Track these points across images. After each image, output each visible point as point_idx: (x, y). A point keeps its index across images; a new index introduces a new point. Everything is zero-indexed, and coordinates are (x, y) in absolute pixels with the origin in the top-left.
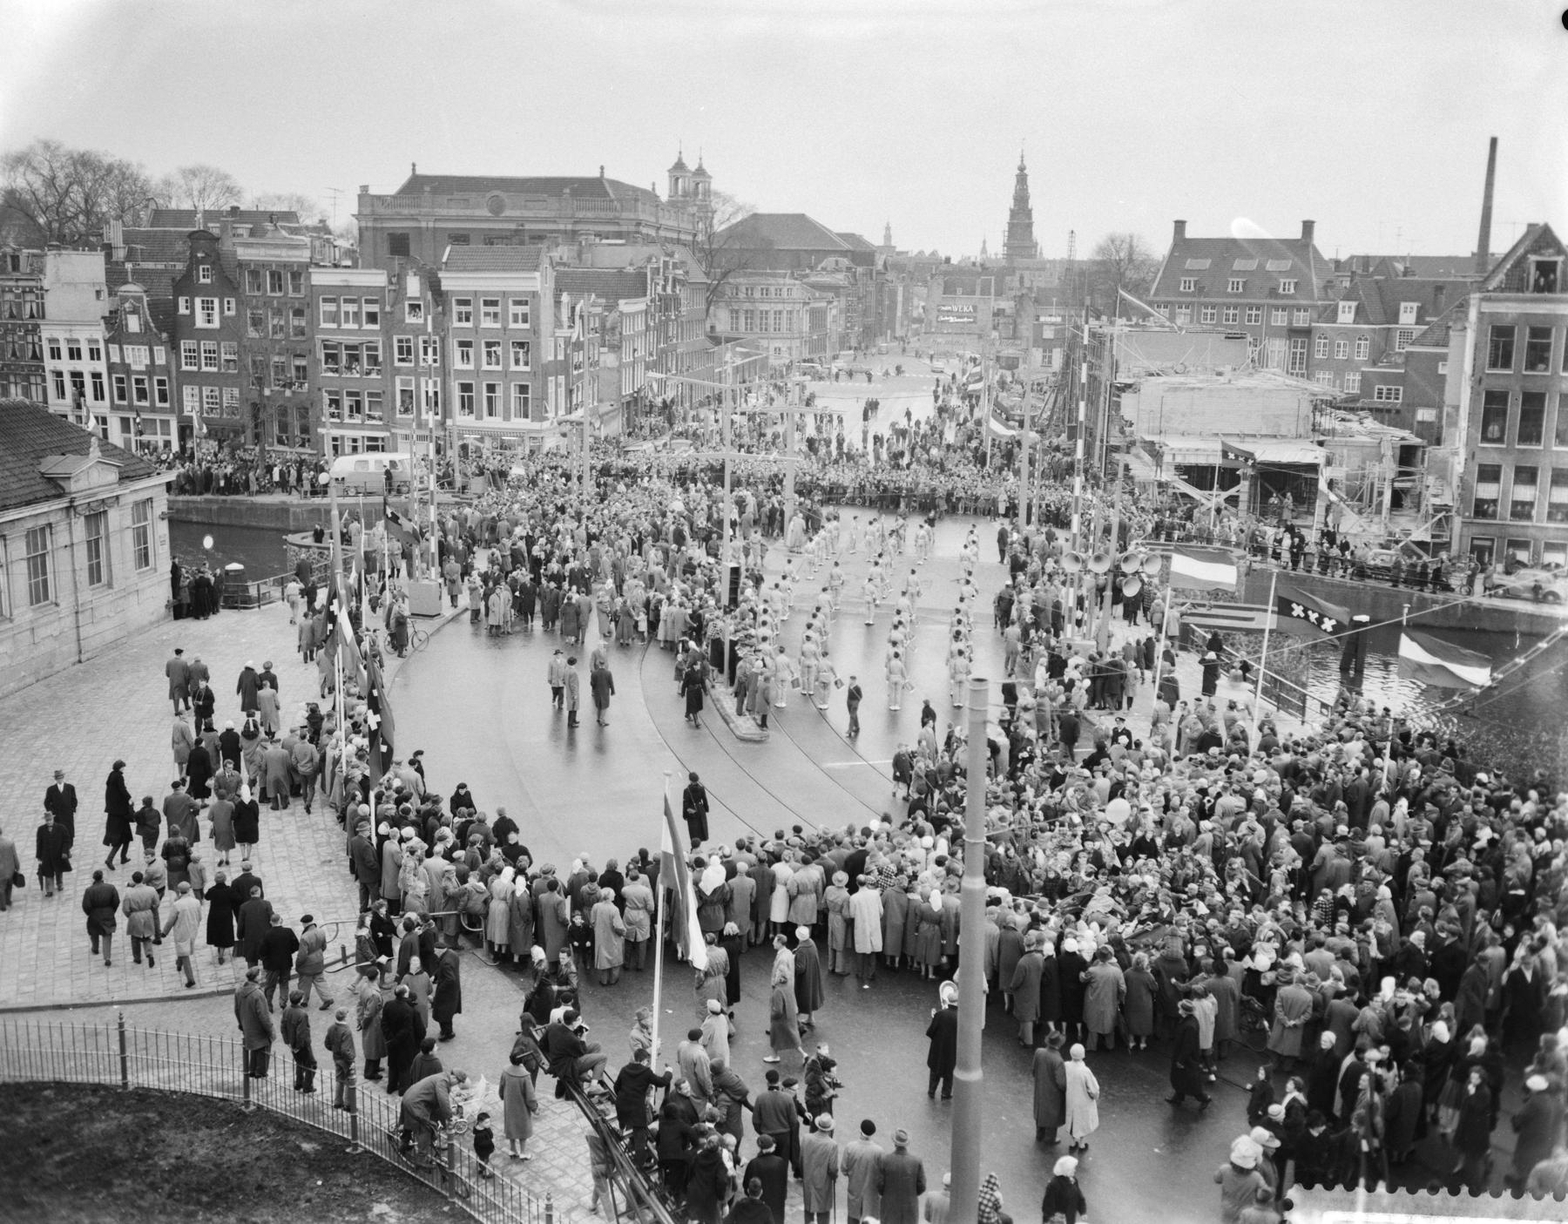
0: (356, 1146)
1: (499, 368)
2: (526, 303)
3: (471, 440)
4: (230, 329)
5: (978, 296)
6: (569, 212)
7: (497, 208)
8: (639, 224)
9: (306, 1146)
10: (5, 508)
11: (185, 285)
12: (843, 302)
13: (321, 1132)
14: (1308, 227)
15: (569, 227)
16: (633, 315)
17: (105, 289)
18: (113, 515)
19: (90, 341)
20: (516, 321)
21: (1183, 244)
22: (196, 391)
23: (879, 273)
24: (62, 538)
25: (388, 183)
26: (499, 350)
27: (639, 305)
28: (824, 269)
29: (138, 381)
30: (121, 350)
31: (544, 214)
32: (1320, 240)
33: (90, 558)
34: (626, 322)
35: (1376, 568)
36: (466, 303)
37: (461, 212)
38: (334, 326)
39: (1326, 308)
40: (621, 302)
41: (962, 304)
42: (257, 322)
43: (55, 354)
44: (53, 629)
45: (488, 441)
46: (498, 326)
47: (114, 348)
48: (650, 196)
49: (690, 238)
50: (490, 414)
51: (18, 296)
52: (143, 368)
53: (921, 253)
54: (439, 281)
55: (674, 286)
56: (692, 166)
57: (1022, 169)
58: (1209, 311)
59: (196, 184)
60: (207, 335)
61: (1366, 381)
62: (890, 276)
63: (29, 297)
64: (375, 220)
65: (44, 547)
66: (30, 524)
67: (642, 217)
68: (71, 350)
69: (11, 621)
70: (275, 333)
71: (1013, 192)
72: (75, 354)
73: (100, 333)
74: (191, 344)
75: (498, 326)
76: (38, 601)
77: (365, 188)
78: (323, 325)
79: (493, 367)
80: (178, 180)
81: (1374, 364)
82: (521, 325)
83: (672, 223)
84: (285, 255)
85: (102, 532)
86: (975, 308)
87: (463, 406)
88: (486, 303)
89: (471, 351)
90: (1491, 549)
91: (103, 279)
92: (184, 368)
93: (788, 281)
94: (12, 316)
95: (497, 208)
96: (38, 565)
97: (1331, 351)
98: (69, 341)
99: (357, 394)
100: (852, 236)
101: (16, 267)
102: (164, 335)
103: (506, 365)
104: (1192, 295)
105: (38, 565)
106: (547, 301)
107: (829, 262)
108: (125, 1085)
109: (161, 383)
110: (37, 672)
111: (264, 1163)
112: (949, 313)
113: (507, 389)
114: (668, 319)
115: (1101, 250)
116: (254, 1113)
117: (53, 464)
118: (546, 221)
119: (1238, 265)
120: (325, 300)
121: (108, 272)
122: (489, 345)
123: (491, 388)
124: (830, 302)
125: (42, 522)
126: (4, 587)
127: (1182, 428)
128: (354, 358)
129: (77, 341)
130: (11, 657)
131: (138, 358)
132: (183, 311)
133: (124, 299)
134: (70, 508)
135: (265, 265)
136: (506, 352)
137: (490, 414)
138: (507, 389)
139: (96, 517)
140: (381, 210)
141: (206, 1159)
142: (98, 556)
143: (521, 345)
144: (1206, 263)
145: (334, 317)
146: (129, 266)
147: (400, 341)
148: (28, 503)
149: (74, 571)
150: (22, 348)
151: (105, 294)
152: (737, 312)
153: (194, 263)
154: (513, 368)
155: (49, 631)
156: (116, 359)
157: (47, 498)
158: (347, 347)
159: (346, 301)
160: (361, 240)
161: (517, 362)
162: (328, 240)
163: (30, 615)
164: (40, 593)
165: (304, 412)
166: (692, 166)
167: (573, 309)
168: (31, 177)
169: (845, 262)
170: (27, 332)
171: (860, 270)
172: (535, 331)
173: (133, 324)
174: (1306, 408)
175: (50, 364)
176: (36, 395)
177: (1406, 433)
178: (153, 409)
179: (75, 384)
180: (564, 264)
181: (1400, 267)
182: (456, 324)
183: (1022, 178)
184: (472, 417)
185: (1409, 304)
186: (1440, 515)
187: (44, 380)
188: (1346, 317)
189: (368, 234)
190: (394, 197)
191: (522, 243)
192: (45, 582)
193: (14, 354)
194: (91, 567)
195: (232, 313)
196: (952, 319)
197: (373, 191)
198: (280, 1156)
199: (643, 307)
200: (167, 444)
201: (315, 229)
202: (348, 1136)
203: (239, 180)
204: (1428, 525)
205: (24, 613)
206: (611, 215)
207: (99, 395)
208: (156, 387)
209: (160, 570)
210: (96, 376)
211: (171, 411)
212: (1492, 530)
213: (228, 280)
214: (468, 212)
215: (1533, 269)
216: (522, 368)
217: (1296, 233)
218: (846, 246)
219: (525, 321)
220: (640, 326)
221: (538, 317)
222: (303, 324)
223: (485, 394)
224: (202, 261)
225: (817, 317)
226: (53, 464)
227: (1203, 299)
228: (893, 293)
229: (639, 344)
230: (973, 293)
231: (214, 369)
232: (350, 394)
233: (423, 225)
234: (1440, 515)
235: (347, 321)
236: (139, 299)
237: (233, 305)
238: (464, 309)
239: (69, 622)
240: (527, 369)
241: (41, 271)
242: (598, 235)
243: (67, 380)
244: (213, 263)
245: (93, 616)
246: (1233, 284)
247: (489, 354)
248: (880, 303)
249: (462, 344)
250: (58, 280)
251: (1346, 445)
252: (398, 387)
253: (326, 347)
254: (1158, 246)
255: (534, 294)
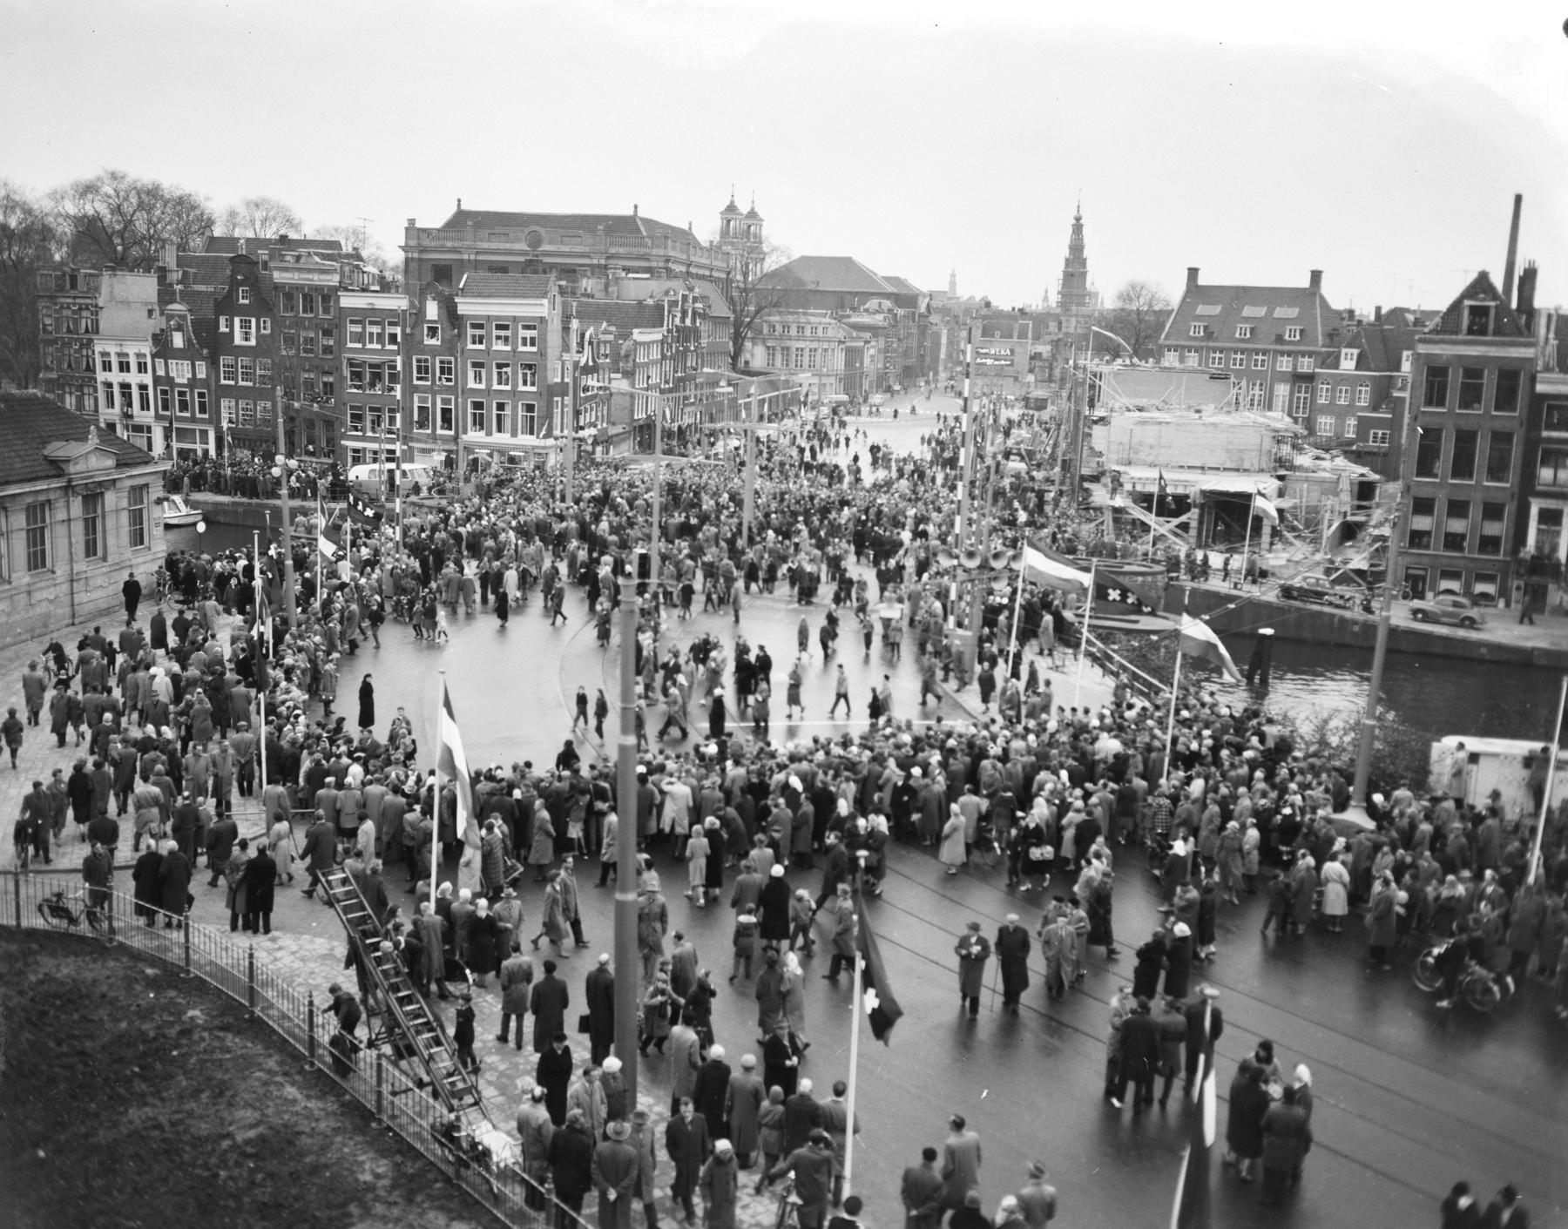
0: (188, 972)
1: (508, 388)
2: (534, 328)
3: (482, 454)
4: (265, 347)
5: (1015, 339)
6: (603, 248)
7: (535, 241)
8: (668, 261)
9: (149, 971)
10: (8, 483)
11: (226, 305)
12: (882, 343)
13: (164, 961)
14: (1316, 276)
15: (603, 262)
16: (648, 344)
17: (156, 307)
18: (110, 498)
19: (138, 355)
20: (525, 344)
21: (1195, 290)
22: (233, 403)
23: (921, 315)
24: (61, 515)
25: (435, 217)
26: (508, 370)
27: (656, 335)
28: (866, 310)
29: (181, 394)
30: (166, 364)
31: (578, 249)
32: (1326, 289)
33: (87, 534)
34: (641, 351)
35: (1300, 589)
36: (481, 326)
37: (502, 246)
38: (359, 346)
39: (1329, 354)
40: (636, 331)
41: (999, 348)
42: (290, 341)
43: (107, 366)
44: (49, 594)
45: (496, 455)
46: (508, 348)
47: (160, 362)
48: (685, 238)
49: (723, 276)
50: (499, 430)
51: (74, 312)
52: (185, 381)
53: (972, 298)
54: (455, 305)
55: (694, 321)
56: (744, 209)
57: (1078, 219)
58: (1217, 355)
59: (259, 215)
60: (243, 351)
61: (1364, 426)
62: (934, 319)
63: (85, 314)
64: (421, 252)
65: (43, 520)
66: (30, 500)
67: (671, 253)
68: (121, 363)
69: (10, 582)
70: (324, 352)
71: (1067, 241)
72: (124, 367)
73: (147, 348)
74: (229, 360)
75: (508, 348)
76: (36, 567)
77: (412, 221)
78: (350, 345)
79: (503, 387)
80: (242, 211)
81: (1375, 408)
82: (529, 349)
83: (704, 261)
84: (317, 279)
85: (99, 511)
86: (1012, 351)
87: (475, 423)
88: (499, 327)
89: (484, 372)
90: (1424, 579)
91: (154, 299)
92: (223, 382)
93: (827, 320)
94: (69, 331)
95: (535, 241)
96: (36, 537)
97: (1333, 398)
98: (119, 355)
99: (378, 410)
100: (897, 279)
101: (74, 286)
102: (205, 351)
103: (515, 385)
104: (1202, 339)
105: (36, 537)
106: (555, 326)
107: (873, 304)
108: (19, 925)
109: (201, 395)
110: (32, 630)
111: (111, 981)
112: (986, 355)
113: (515, 408)
114: (687, 350)
115: (1126, 297)
116: (115, 948)
117: (57, 449)
118: (582, 255)
119: (1248, 311)
120: (352, 322)
121: (160, 293)
122: (499, 366)
123: (501, 407)
124: (867, 342)
125: (42, 498)
126: (4, 551)
127: (1150, 459)
128: (377, 377)
129: (127, 355)
130: (9, 615)
131: (181, 372)
132: (223, 329)
133: (170, 318)
134: (68, 489)
135: (299, 288)
136: (515, 373)
137: (499, 430)
138: (515, 408)
139: (93, 496)
140: (426, 243)
141: (68, 976)
142: (94, 532)
143: (530, 367)
144: (1216, 310)
145: (359, 338)
146: (179, 287)
147: (419, 361)
148: (30, 480)
149: (70, 543)
150: (78, 362)
151: (156, 314)
152: (774, 349)
153: (234, 285)
154: (521, 388)
155: (45, 594)
156: (161, 372)
157: (47, 477)
158: (371, 366)
159: (371, 323)
160: (407, 271)
161: (525, 383)
162: (357, 267)
163: (27, 580)
164: (37, 560)
165: (329, 424)
166: (744, 209)
167: (583, 335)
168: (97, 205)
169: (887, 304)
170: (82, 345)
171: (900, 312)
172: (542, 354)
173: (178, 340)
174: (1268, 443)
175: (101, 376)
176: (88, 403)
177: (1365, 470)
178: (193, 419)
179: (123, 394)
180: (588, 296)
181: (1411, 318)
182: (470, 346)
183: (1078, 228)
184: (483, 433)
185: (1349, 351)
186: (1377, 545)
187: (96, 391)
188: (1348, 364)
189: (414, 265)
190: (439, 230)
191: (536, 272)
192: (43, 551)
193: (70, 366)
194: (87, 542)
195: (268, 332)
196: (989, 362)
197: (418, 225)
198: (126, 977)
199: (659, 337)
200: (206, 452)
201: (348, 256)
202: (182, 964)
203: (298, 213)
204: (1366, 554)
205: (22, 577)
206: (643, 251)
207: (145, 406)
208: (470, 410)
209: (154, 549)
210: (143, 387)
211: (209, 422)
212: (1425, 560)
213: (266, 300)
214: (508, 246)
215: (1466, 314)
216: (529, 388)
217: (1305, 282)
218: (890, 289)
219: (533, 344)
220: (655, 354)
221: (545, 341)
222: (331, 342)
223: (495, 412)
224: (242, 283)
225: (853, 355)
226: (57, 449)
227: (1211, 344)
228: (937, 336)
229: (654, 372)
230: (1011, 336)
231: (250, 384)
232: (372, 409)
233: (466, 257)
234: (1377, 545)
235: (371, 342)
236: (183, 317)
237: (269, 324)
238: (478, 332)
239: (65, 588)
240: (534, 389)
241: (97, 289)
242: (628, 270)
243: (116, 390)
244: (251, 286)
245: (87, 584)
246: (1241, 331)
247: (499, 374)
248: (921, 345)
249: (475, 365)
250: (112, 299)
251: (1307, 480)
252: (416, 404)
253: (352, 365)
254: (1172, 292)
255: (542, 320)
